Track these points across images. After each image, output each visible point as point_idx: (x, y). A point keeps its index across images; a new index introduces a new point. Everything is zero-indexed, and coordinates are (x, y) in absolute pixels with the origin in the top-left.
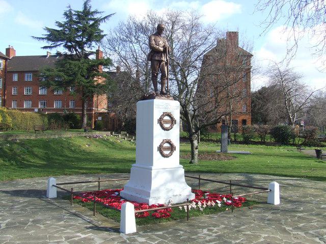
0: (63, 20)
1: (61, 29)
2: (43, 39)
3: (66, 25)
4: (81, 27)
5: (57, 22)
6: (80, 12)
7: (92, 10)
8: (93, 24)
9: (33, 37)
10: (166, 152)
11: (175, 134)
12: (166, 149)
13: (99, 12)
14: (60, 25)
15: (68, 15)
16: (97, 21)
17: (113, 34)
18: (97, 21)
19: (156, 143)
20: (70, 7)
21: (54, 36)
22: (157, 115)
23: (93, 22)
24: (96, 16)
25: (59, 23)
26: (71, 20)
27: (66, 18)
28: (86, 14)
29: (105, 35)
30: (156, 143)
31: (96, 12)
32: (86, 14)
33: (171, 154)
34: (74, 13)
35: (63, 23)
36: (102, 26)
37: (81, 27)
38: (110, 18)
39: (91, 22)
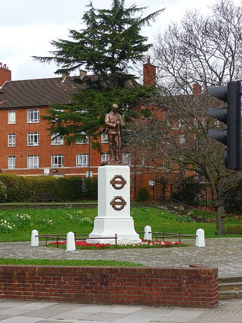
0: (81, 26)
1: (77, 41)
2: (50, 59)
3: (86, 36)
4: (113, 35)
5: (72, 32)
6: (108, 11)
7: (126, 6)
8: (130, 30)
9: (35, 57)
10: (118, 206)
11: (125, 193)
12: (118, 204)
13: (138, 9)
14: (76, 34)
15: (89, 17)
16: (136, 25)
17: (163, 42)
18: (136, 25)
19: (127, 187)
20: (91, 5)
21: (69, 51)
22: (110, 177)
23: (129, 26)
24: (135, 16)
25: (76, 32)
26: (95, 26)
27: (87, 24)
28: (118, 14)
29: (150, 46)
30: (110, 198)
31: (134, 9)
32: (118, 14)
33: (122, 208)
34: (97, 13)
35: (81, 32)
36: (144, 31)
37: (113, 35)
38: (157, 18)
39: (126, 27)
